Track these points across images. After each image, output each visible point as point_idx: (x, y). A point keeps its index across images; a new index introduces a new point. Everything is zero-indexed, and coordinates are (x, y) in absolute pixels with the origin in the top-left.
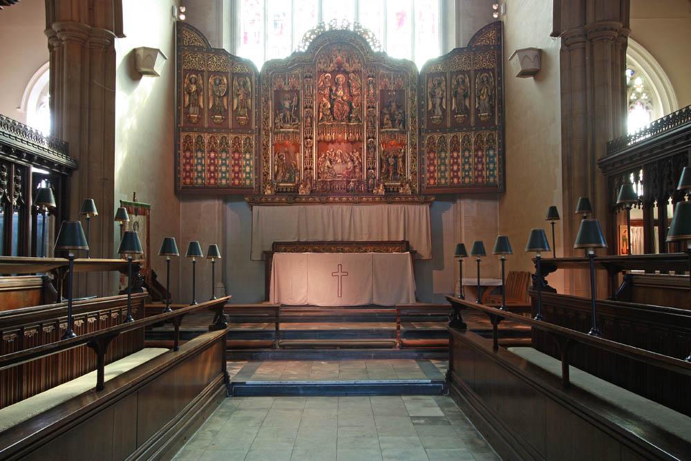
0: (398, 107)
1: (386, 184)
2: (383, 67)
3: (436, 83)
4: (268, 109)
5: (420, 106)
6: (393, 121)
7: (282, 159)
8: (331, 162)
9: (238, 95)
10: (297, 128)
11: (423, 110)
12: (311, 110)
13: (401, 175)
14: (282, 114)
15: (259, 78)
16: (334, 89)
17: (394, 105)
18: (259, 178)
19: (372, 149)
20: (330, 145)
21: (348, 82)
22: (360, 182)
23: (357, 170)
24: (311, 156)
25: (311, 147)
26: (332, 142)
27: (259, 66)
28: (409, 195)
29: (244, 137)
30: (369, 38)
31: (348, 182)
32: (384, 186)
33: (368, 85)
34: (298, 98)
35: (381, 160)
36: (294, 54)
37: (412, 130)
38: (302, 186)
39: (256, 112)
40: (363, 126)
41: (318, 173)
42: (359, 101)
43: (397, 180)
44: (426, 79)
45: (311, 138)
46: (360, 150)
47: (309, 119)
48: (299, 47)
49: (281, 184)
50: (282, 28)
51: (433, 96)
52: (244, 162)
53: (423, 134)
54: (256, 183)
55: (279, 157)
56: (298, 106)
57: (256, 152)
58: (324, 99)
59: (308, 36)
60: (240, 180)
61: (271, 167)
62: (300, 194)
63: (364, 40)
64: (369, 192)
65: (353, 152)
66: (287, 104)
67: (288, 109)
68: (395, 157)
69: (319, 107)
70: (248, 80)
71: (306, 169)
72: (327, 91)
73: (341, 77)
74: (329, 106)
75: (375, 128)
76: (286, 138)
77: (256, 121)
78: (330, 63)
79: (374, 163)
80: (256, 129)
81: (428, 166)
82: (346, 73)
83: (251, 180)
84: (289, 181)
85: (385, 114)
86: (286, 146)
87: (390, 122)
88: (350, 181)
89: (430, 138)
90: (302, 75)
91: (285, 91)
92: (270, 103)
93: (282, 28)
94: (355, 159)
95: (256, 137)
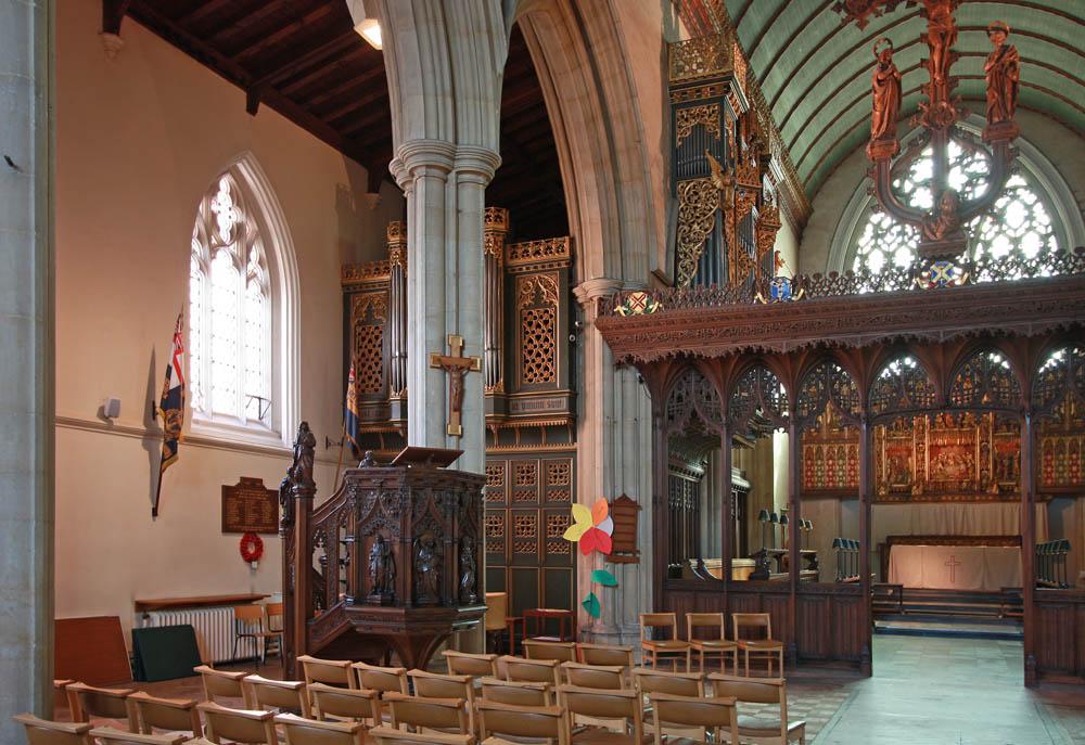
20: (942, 449)
22: (973, 482)
31: (961, 482)
45: (923, 444)
46: (973, 452)
64: (982, 491)
79: (987, 464)
83: (1064, 478)
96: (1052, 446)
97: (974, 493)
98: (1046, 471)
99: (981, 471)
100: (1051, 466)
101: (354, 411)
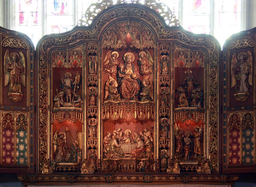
0: (195, 86)
1: (181, 163)
2: (178, 44)
3: (242, 58)
4: (45, 85)
5: (222, 83)
6: (190, 100)
7: (62, 139)
8: (118, 142)
9: (9, 70)
10: (80, 107)
11: (225, 87)
12: (95, 88)
13: (198, 155)
14: (62, 93)
15: (35, 53)
16: (122, 67)
17: (190, 83)
18: (35, 156)
19: (166, 128)
20: (117, 125)
21: (138, 61)
22: (151, 161)
23: (148, 150)
24: (96, 135)
25: (96, 127)
26: (120, 121)
27: (35, 42)
28: (209, 174)
29: (18, 114)
30: (163, 12)
31: (138, 162)
32: (180, 165)
33: (161, 63)
34: (81, 77)
35: (175, 140)
36: (76, 28)
37: (211, 108)
38: (84, 165)
39: (31, 89)
40: (155, 105)
41: (104, 153)
42: (151, 80)
43: (192, 159)
44: (229, 55)
45: (95, 117)
46: (152, 129)
47: (93, 98)
48: (82, 17)
49: (61, 164)
50: (63, 7)
51: (237, 72)
52: (18, 140)
53: (225, 112)
54: (31, 162)
55: (58, 136)
56: (80, 83)
57: (31, 129)
58: (110, 77)
59: (92, 10)
60: (12, 158)
61: (49, 145)
62: (82, 173)
63: (158, 15)
64: (161, 171)
65: (143, 132)
66: (68, 82)
67: (68, 87)
68: (192, 137)
69: (105, 85)
70: (22, 54)
71: (90, 148)
72: (114, 70)
73: (130, 56)
74: (116, 85)
75: (169, 107)
76: (67, 116)
77: (31, 97)
78: (118, 39)
79: (167, 142)
80: (31, 106)
81: (231, 145)
82: (136, 51)
83: (25, 159)
84: (71, 160)
85: (181, 92)
86: (67, 125)
87: (186, 101)
88: (140, 161)
89: (232, 116)
90: (86, 51)
91: (66, 69)
92: (48, 80)
93: (63, 7)
94: (146, 139)
95: (31, 114)
96: (238, 122)
97: (151, 172)
98: (231, 150)
99: (161, 149)
100: (10, 143)
101: (150, 14)
